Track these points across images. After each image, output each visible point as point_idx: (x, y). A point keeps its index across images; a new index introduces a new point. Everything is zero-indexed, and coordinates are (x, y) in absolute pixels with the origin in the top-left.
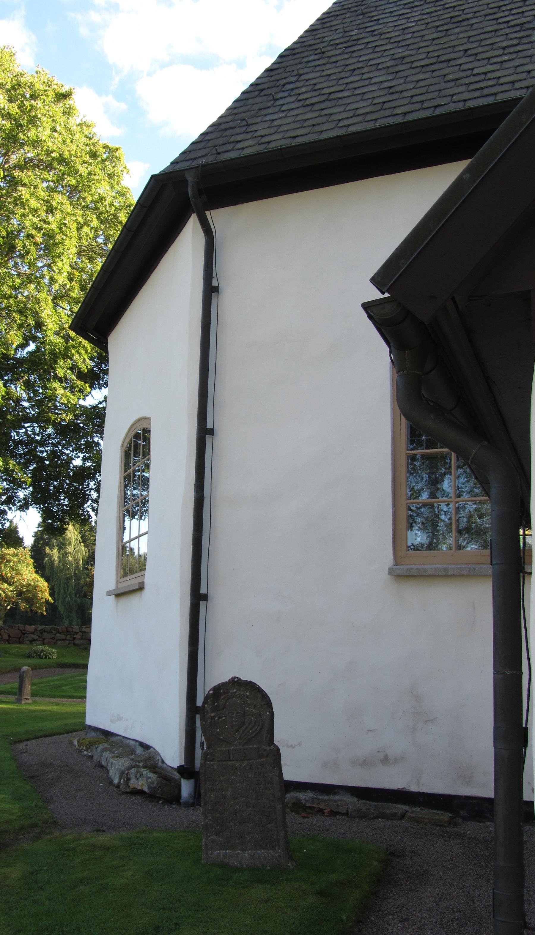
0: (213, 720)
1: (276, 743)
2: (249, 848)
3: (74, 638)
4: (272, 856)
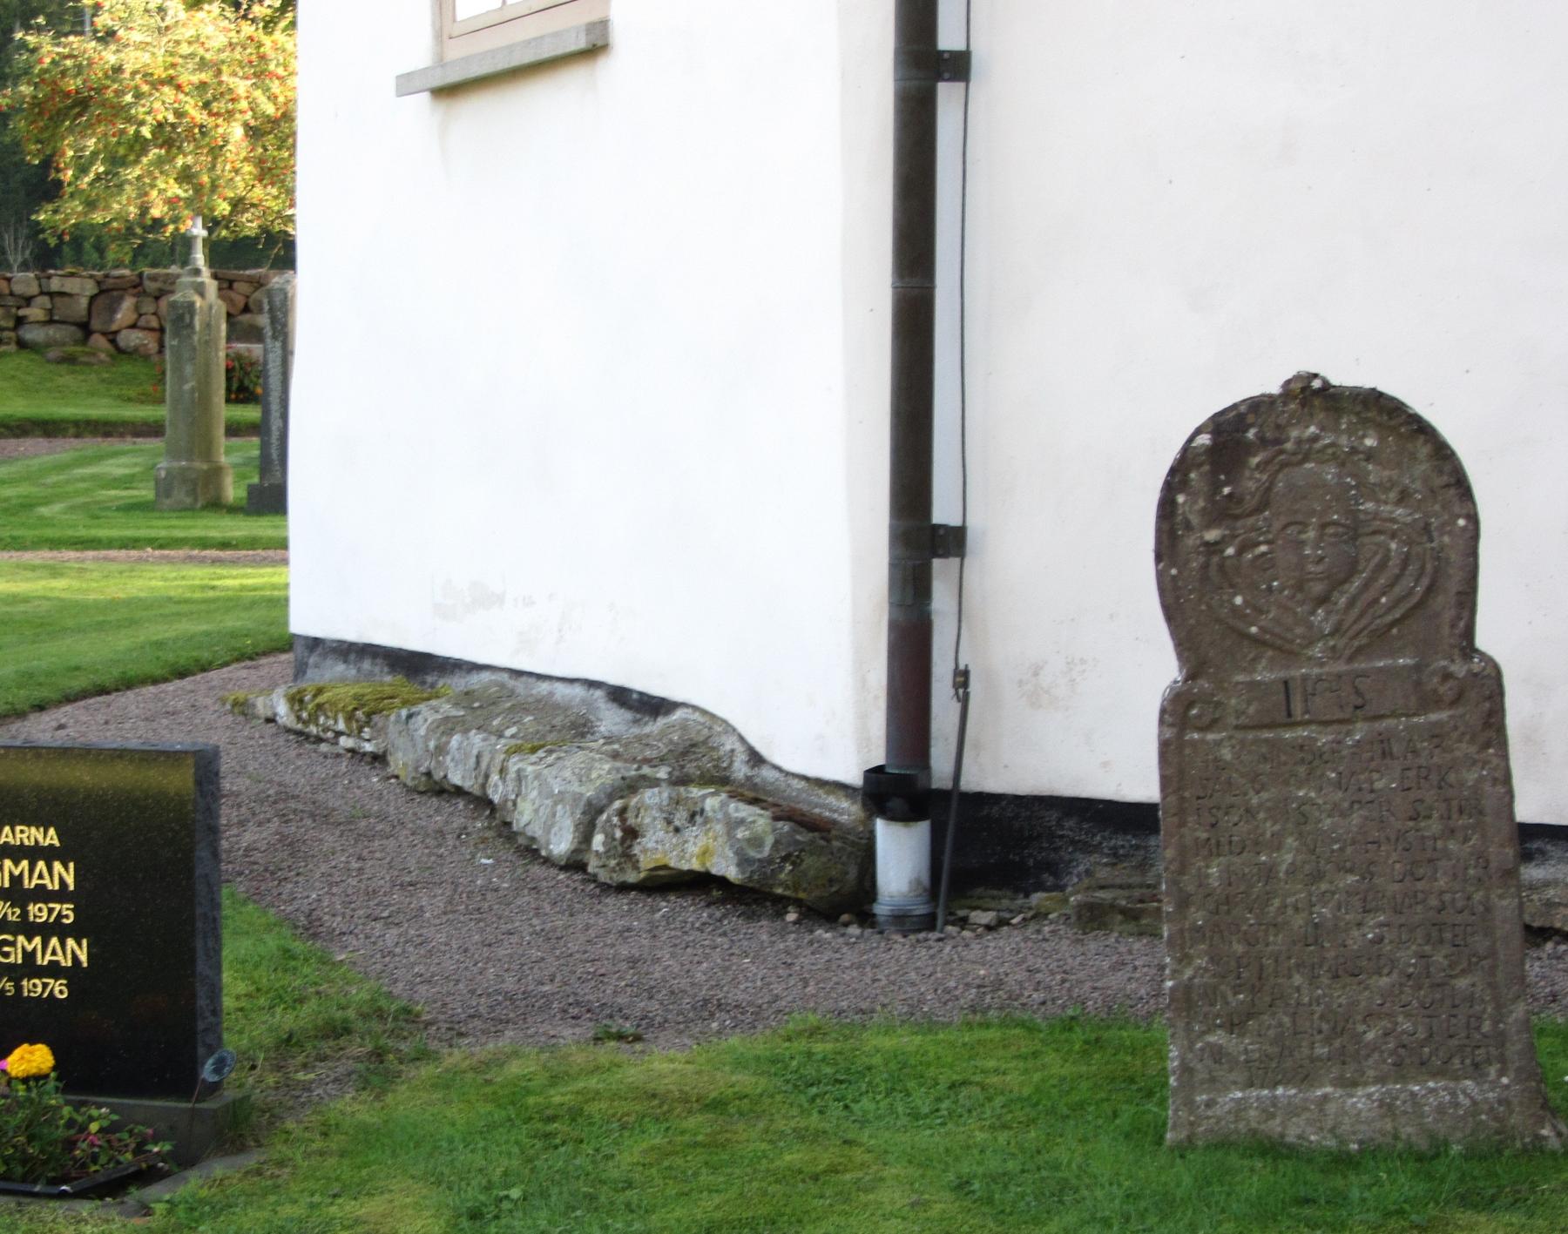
0: (1215, 559)
1: (1482, 641)
2: (1371, 1073)
3: (20, 321)
4: (1475, 1103)
